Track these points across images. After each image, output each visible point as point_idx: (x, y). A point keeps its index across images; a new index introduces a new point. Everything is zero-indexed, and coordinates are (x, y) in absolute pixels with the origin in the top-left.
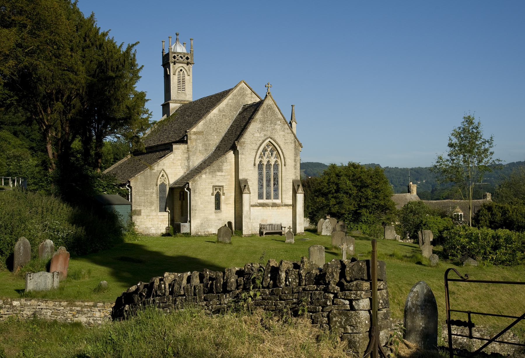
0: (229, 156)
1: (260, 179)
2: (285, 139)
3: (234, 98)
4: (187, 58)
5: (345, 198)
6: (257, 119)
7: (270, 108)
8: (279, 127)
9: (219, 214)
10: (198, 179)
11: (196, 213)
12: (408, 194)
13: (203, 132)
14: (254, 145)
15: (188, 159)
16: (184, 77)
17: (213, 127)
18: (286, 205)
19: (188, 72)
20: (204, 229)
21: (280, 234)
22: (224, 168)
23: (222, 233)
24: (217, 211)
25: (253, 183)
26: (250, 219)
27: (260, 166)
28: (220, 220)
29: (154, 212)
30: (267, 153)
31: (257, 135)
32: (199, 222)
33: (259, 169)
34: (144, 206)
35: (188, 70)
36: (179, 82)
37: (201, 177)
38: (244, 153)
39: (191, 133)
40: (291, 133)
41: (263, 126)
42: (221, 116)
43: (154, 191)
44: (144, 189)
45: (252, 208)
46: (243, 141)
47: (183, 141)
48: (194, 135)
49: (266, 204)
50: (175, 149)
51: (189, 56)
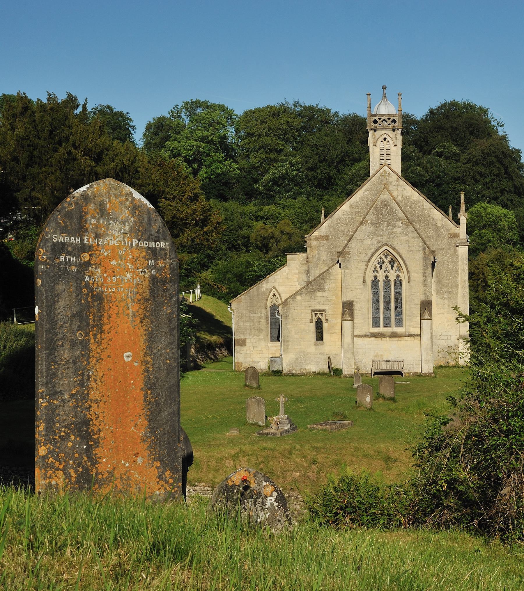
0: (334, 271)
1: (376, 301)
2: (409, 246)
3: (371, 188)
6: (367, 221)
7: (385, 205)
8: (400, 229)
9: (320, 347)
10: (291, 302)
11: (288, 345)
13: (327, 236)
14: (362, 256)
15: (308, 272)
16: (389, 148)
17: (341, 229)
18: (410, 335)
19: (395, 141)
22: (327, 286)
24: (318, 342)
25: (362, 307)
26: (353, 353)
27: (375, 283)
28: (321, 354)
29: (263, 341)
32: (293, 356)
33: (374, 287)
36: (382, 156)
37: (295, 298)
38: (348, 266)
40: (417, 237)
41: (376, 230)
42: (354, 214)
43: (263, 315)
44: (250, 312)
46: (347, 250)
47: (301, 249)
48: (316, 240)
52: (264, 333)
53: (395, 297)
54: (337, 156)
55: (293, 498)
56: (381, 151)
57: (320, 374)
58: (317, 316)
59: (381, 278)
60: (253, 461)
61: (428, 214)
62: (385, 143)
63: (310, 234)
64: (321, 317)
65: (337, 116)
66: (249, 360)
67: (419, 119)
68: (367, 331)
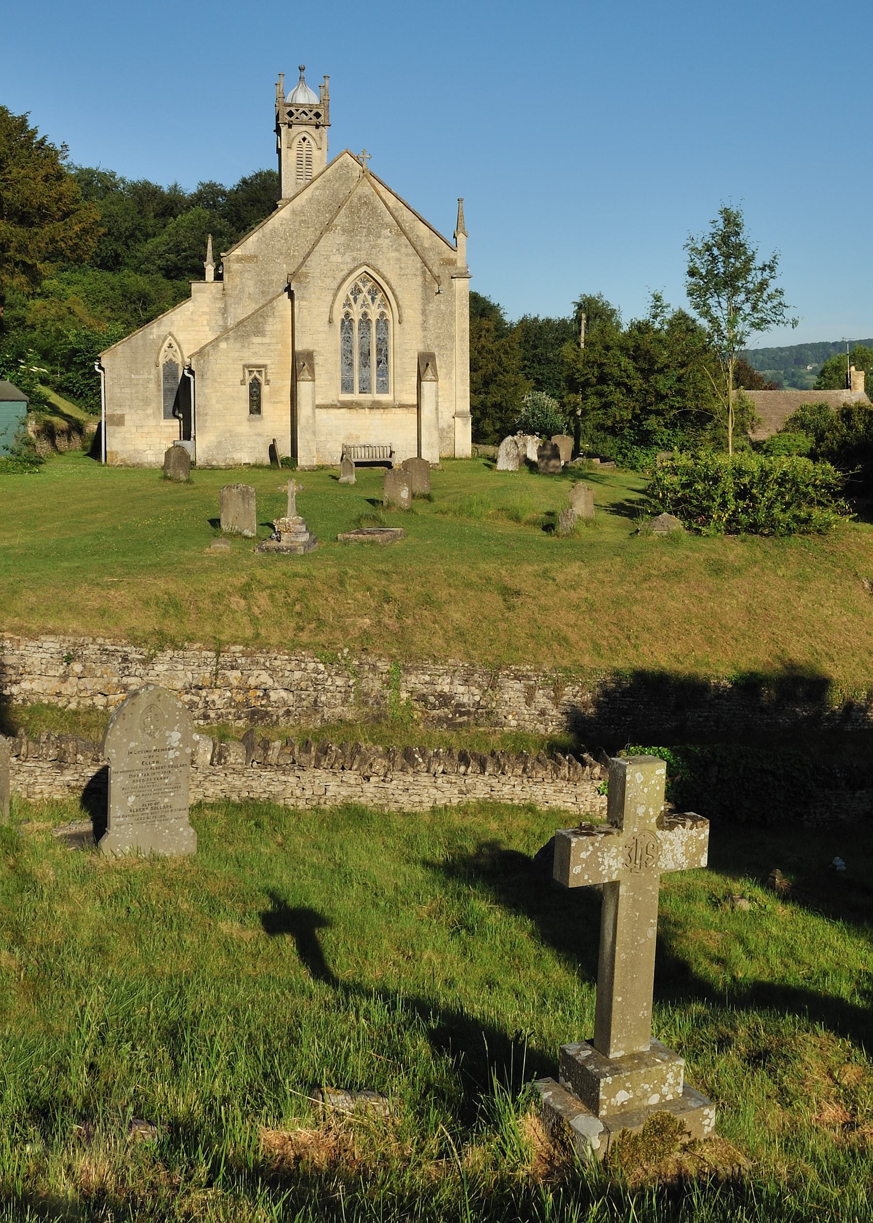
0: (280, 304)
1: (347, 354)
4: (318, 115)
5: (617, 396)
6: (336, 226)
7: (365, 202)
8: (387, 241)
9: (258, 424)
10: (211, 352)
11: (205, 421)
12: (845, 392)
13: (256, 257)
14: (328, 281)
15: (224, 311)
17: (278, 246)
18: (402, 406)
19: (318, 142)
20: (225, 454)
21: (388, 465)
22: (268, 328)
23: (172, 461)
26: (314, 433)
29: (151, 418)
30: (361, 297)
31: (338, 258)
32: (213, 439)
34: (130, 406)
35: (317, 139)
36: (299, 163)
37: (218, 346)
39: (231, 259)
42: (297, 224)
43: (152, 377)
44: (131, 372)
45: (317, 411)
48: (238, 262)
49: (357, 403)
50: (196, 292)
51: (320, 111)
52: (153, 404)
53: (377, 346)
54: (127, 229)
55: (367, 667)
56: (299, 156)
57: (257, 466)
58: (253, 376)
59: (356, 317)
60: (279, 596)
61: (411, 228)
62: (305, 144)
63: (228, 252)
64: (258, 376)
65: (124, 183)
66: (129, 447)
67: (228, 189)
68: (335, 398)
